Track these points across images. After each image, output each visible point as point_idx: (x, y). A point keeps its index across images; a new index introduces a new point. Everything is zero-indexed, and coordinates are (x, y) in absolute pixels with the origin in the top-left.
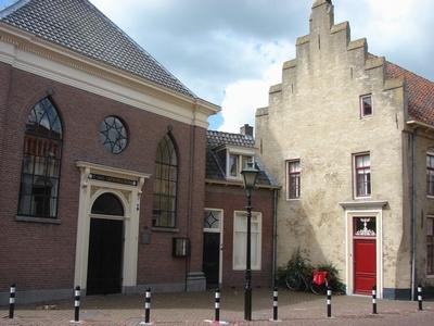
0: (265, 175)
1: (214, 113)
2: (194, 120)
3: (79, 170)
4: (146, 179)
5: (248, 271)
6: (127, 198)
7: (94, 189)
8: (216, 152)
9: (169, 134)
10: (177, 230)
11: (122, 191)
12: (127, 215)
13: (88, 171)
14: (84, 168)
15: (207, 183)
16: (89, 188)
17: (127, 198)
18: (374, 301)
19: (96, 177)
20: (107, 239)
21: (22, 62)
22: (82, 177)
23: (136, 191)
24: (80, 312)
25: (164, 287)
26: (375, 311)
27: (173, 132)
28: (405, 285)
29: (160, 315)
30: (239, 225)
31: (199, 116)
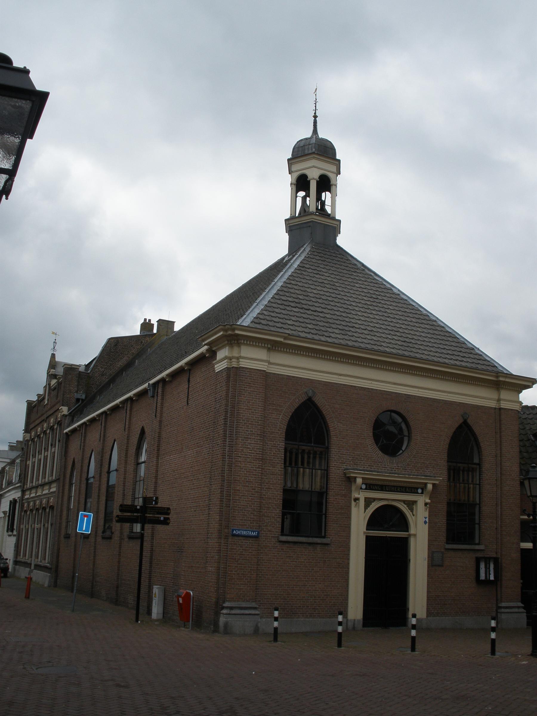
4: (434, 485)
6: (412, 510)
7: (368, 502)
10: (482, 547)
11: (404, 502)
12: (412, 531)
13: (359, 481)
14: (355, 478)
16: (362, 502)
17: (412, 510)
18: (276, 624)
19: (370, 486)
22: (353, 488)
23: (422, 500)
27: (469, 421)
31: (505, 395)
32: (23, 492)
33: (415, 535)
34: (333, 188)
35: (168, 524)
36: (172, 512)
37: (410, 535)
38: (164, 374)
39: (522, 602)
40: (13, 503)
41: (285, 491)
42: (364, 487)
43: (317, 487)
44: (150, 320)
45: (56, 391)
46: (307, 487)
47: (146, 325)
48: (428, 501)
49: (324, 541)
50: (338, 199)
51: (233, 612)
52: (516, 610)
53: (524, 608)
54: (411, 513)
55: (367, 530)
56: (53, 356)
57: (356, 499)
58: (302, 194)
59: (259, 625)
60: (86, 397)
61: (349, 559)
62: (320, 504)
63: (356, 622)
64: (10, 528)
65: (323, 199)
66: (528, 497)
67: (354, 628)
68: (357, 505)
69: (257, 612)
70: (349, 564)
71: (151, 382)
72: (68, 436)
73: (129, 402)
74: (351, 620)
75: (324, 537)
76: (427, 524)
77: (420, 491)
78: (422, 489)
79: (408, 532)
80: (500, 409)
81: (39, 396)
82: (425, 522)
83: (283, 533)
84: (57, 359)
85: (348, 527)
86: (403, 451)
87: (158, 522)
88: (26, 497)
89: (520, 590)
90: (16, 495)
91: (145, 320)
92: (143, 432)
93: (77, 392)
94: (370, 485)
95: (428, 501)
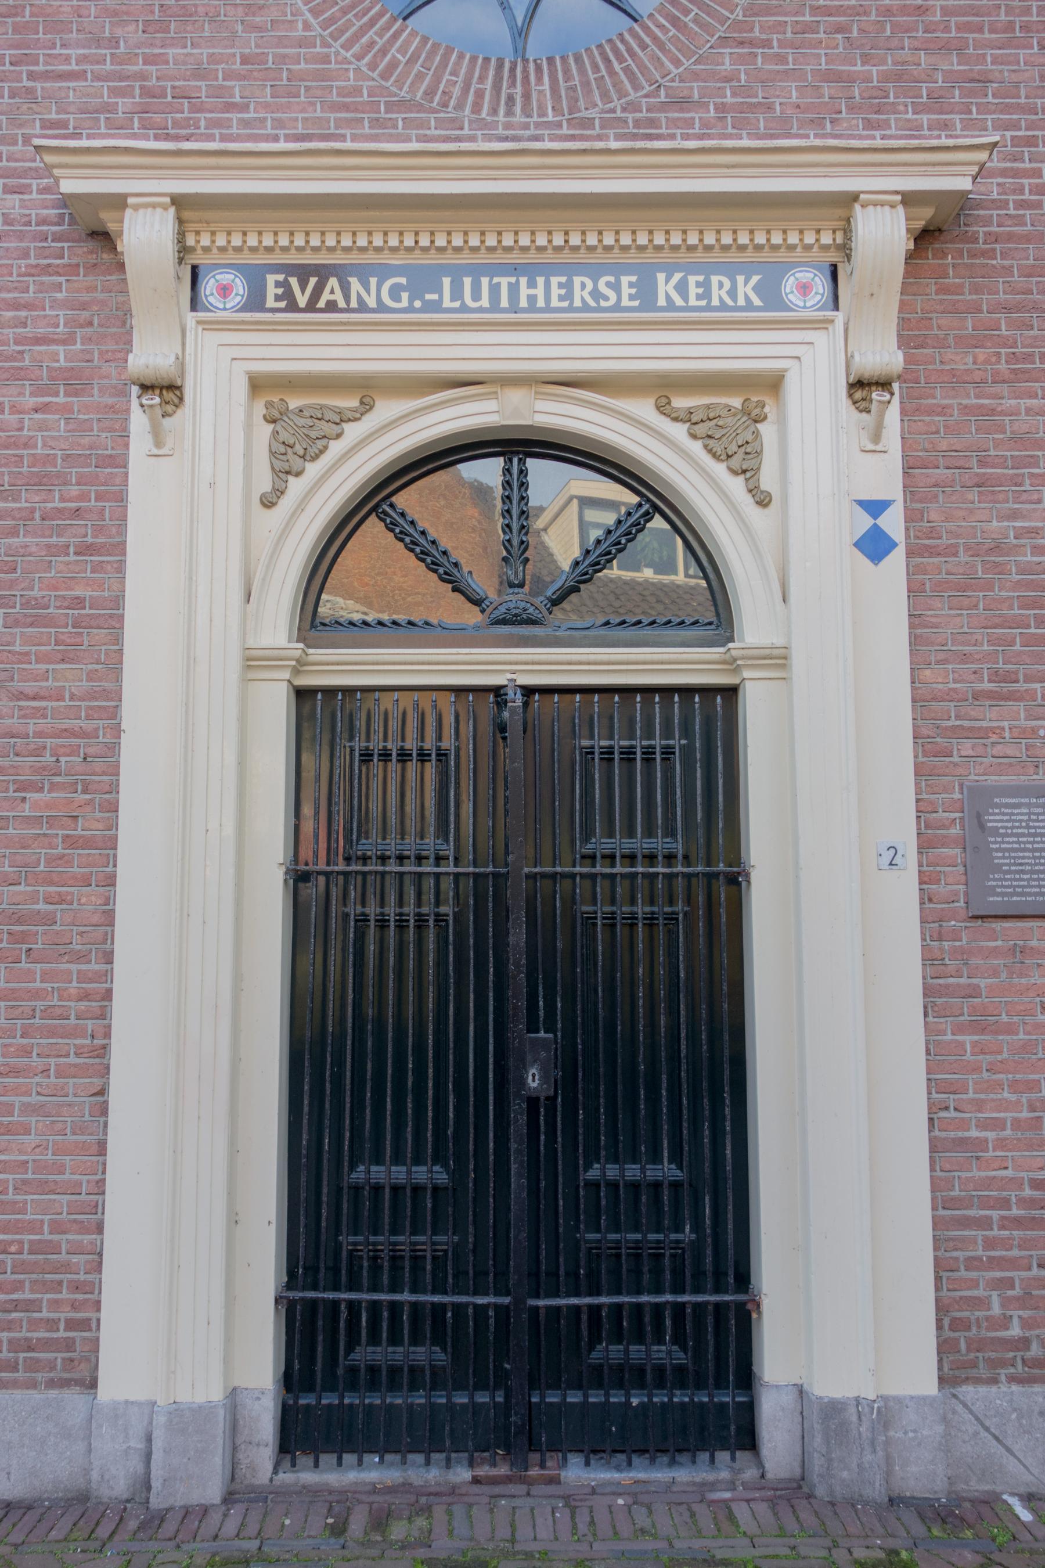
11: (662, 388)
12: (756, 624)
33: (778, 660)
48: (883, 354)
54: (736, 486)
57: (167, 391)
63: (160, 1420)
74: (120, 1411)
76: (897, 559)
82: (874, 546)
85: (101, 621)
92: (386, 713)
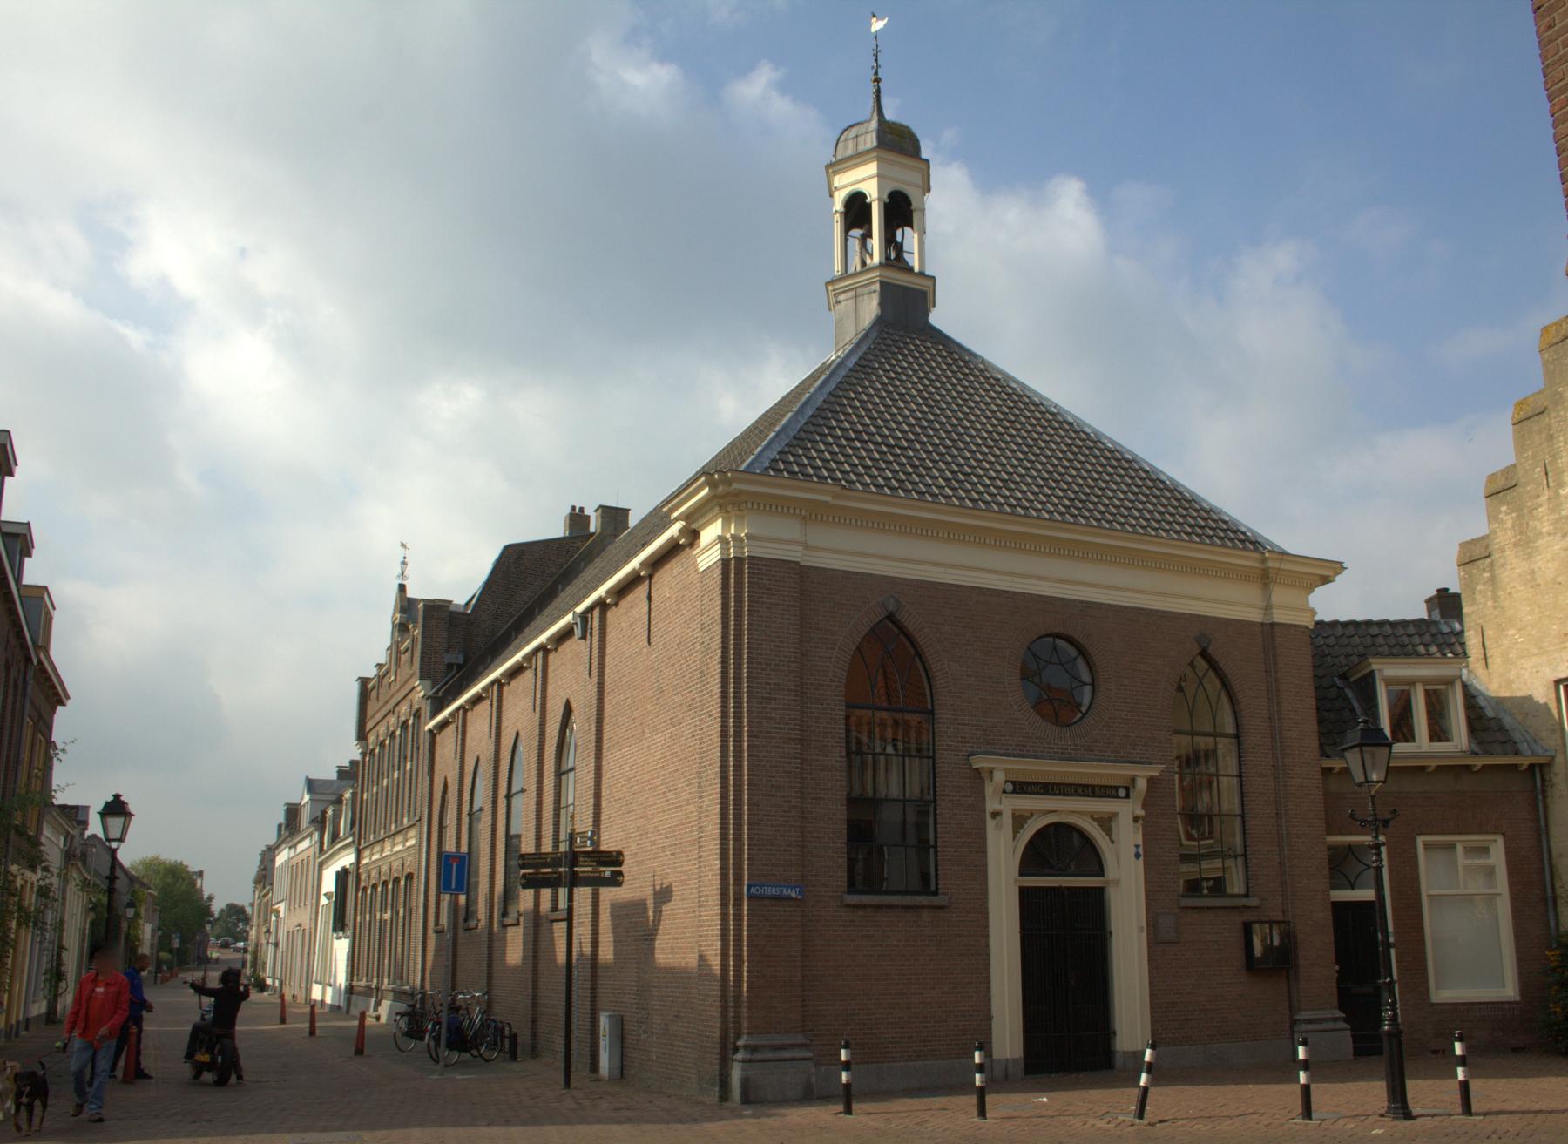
0: (1502, 729)
1: (1326, 580)
2: (1268, 608)
3: (978, 778)
4: (1151, 780)
5: (323, 1002)
7: (1019, 820)
8: (1345, 672)
9: (1204, 654)
10: (1253, 902)
12: (1111, 871)
13: (1000, 777)
14: (991, 772)
15: (1327, 771)
16: (1007, 820)
19: (1021, 787)
20: (1066, 939)
21: (1183, 597)
22: (989, 789)
23: (1126, 811)
24: (989, 1098)
25: (1202, 1046)
26: (1467, 1108)
27: (1210, 651)
28: (497, 1008)
29: (866, 1116)
30: (1433, 876)
32: (359, 853)
34: (916, 217)
35: (619, 884)
36: (628, 860)
37: (1108, 882)
38: (601, 591)
39: (1341, 1008)
40: (342, 876)
41: (852, 802)
42: (1010, 787)
43: (913, 791)
44: (582, 509)
45: (408, 654)
46: (895, 791)
47: (577, 518)
48: (1140, 812)
49: (936, 900)
50: (928, 238)
51: (759, 1056)
52: (1330, 1025)
53: (1346, 1020)
55: (1021, 874)
56: (402, 588)
57: (995, 815)
58: (857, 232)
59: (813, 1080)
60: (466, 661)
61: (987, 936)
62: (921, 827)
64: (339, 924)
65: (899, 239)
66: (1360, 785)
67: (1006, 1077)
68: (999, 827)
69: (809, 1055)
70: (987, 945)
71: (580, 609)
72: (433, 734)
73: (540, 654)
75: (936, 893)
77: (1122, 792)
78: (1127, 789)
79: (1102, 875)
80: (1273, 625)
81: (379, 666)
82: (1137, 856)
83: (852, 887)
84: (410, 594)
86: (1084, 715)
87: (597, 882)
88: (365, 861)
89: (1334, 984)
90: (347, 859)
91: (573, 508)
93: (447, 651)
94: (1022, 783)
95: (1140, 812)
